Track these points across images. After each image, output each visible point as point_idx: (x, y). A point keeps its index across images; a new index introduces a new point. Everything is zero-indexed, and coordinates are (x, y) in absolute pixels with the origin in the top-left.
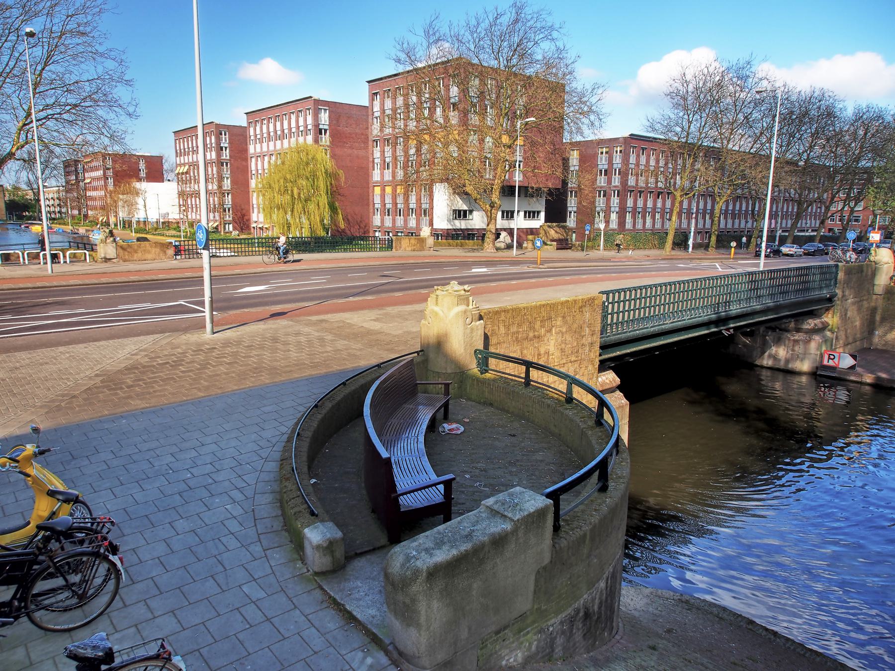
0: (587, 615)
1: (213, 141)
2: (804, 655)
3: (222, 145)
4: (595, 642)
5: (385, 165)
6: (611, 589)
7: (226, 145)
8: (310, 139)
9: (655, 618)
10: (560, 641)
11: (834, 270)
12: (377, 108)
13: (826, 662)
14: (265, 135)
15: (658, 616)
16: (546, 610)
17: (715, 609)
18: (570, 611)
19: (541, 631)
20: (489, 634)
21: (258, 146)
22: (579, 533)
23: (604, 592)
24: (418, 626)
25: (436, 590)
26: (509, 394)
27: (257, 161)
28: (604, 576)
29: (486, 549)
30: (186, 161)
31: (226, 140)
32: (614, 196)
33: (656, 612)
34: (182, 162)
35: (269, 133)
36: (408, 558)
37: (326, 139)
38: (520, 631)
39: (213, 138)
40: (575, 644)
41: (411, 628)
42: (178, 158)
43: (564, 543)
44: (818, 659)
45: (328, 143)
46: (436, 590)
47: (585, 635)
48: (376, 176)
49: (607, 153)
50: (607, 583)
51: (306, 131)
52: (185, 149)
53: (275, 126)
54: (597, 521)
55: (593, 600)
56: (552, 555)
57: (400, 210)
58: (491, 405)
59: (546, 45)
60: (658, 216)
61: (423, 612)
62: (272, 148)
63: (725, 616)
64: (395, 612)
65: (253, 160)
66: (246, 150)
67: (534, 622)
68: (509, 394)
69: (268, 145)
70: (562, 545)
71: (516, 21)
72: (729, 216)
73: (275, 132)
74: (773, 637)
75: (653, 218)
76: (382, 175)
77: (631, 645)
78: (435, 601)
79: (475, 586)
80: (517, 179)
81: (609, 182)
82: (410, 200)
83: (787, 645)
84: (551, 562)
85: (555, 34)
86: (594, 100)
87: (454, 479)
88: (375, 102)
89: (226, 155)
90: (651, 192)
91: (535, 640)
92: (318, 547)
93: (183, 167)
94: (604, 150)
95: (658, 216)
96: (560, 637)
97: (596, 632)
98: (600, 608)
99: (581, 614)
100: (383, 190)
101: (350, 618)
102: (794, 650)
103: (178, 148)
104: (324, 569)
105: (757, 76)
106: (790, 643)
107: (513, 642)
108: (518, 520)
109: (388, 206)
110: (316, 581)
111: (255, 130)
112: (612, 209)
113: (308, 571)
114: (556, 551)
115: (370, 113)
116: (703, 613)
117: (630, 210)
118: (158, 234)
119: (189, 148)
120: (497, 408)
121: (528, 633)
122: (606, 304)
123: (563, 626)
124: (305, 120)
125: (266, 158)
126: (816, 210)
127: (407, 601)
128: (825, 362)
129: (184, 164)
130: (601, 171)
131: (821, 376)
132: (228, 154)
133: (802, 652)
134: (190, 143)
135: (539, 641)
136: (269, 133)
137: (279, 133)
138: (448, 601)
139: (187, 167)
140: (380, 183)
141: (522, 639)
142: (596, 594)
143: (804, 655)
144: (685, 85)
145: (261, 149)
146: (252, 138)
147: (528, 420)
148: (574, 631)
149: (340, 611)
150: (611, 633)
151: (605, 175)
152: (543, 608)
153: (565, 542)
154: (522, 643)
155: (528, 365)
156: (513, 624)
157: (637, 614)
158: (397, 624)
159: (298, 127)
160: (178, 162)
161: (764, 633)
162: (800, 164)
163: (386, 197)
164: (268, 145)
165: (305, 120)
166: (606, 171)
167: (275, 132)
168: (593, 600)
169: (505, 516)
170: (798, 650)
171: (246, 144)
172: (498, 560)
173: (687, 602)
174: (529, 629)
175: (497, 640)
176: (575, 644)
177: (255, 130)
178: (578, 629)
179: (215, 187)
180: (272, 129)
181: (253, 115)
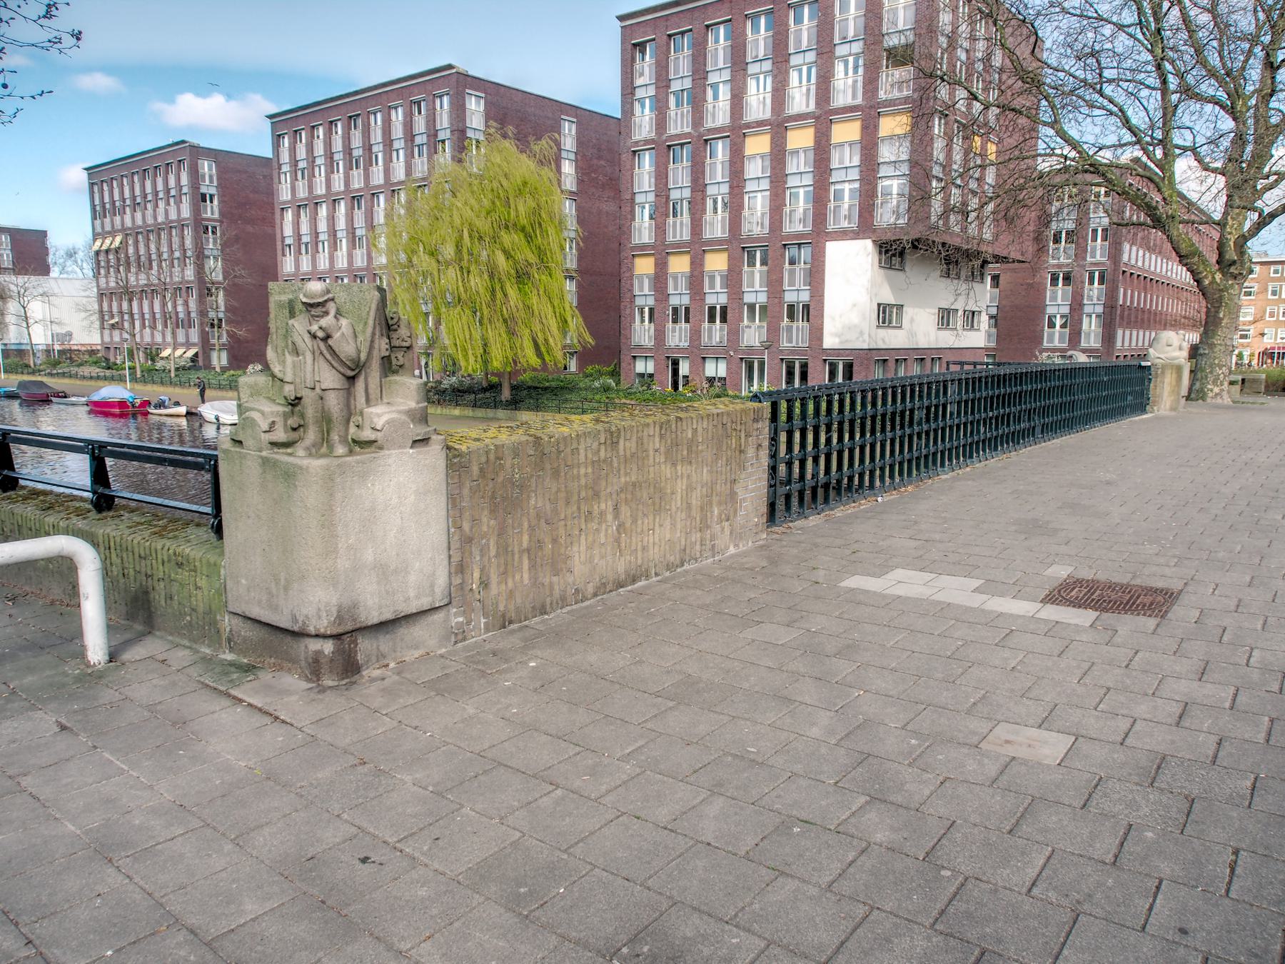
3: (203, 190)
7: (213, 191)
12: (285, 157)
27: (297, 216)
31: (211, 181)
32: (643, 321)
42: (98, 222)
65: (289, 216)
89: (212, 211)
93: (108, 242)
103: (97, 202)
115: (275, 165)
118: (63, 375)
119: (124, 200)
125: (323, 211)
129: (113, 233)
132: (216, 210)
139: (118, 239)
146: (285, 168)
151: (724, 320)
160: (99, 229)
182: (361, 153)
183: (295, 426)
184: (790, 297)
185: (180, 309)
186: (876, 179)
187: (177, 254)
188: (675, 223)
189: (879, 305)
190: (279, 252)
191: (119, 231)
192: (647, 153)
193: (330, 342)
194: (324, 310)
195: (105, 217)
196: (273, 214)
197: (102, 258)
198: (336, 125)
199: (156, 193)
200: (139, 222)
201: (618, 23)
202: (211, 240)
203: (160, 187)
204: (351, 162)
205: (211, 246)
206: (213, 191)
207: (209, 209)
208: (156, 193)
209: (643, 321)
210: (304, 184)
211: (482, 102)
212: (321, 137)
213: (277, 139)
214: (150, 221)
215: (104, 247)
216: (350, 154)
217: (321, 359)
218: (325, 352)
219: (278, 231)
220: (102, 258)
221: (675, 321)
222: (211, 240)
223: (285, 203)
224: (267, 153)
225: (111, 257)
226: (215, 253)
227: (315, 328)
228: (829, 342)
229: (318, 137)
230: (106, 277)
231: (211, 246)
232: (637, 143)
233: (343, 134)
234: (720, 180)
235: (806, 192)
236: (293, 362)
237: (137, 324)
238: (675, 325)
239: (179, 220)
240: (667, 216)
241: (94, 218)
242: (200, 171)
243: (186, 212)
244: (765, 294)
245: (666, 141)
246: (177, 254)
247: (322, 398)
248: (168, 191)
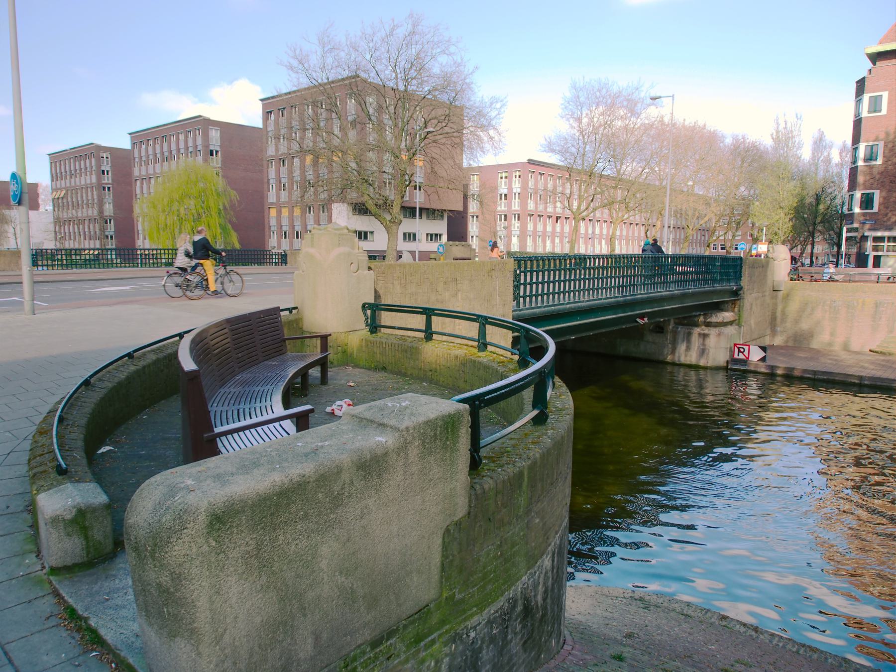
0: (528, 611)
1: (93, 164)
2: (797, 652)
4: (539, 656)
5: (281, 186)
6: (557, 572)
7: (109, 169)
8: (200, 158)
9: (606, 622)
10: (487, 654)
11: (739, 261)
13: (826, 659)
14: (151, 157)
15: (609, 619)
16: (462, 601)
17: (676, 605)
18: (501, 603)
19: (456, 638)
20: (359, 646)
21: (143, 168)
22: (511, 470)
23: (550, 574)
24: (193, 633)
25: (234, 554)
26: (406, 351)
27: (142, 184)
28: (550, 548)
29: (345, 477)
30: (63, 186)
31: (107, 164)
32: (515, 220)
33: (606, 614)
34: (59, 186)
35: (155, 155)
36: (172, 491)
37: (217, 161)
38: (418, 639)
39: (93, 160)
40: (510, 659)
41: (178, 639)
42: (54, 183)
43: (488, 483)
44: (815, 656)
45: (220, 165)
46: (234, 554)
47: (525, 642)
48: (271, 197)
49: (506, 177)
50: (553, 561)
51: (196, 151)
52: (61, 173)
53: (162, 148)
54: (538, 455)
55: (535, 586)
56: (470, 501)
57: (297, 232)
58: (384, 369)
59: (443, 59)
60: (557, 240)
61: (202, 603)
62: (158, 170)
63: (690, 612)
64: (147, 611)
65: (138, 183)
66: (129, 174)
67: (443, 622)
68: (406, 351)
69: (154, 167)
70: (486, 487)
71: (413, 33)
72: (623, 242)
73: (163, 153)
74: (754, 633)
75: (553, 242)
76: (278, 196)
77: (588, 657)
78: (234, 579)
79: (324, 550)
80: (418, 200)
81: (510, 206)
82: (307, 221)
83: (775, 642)
84: (469, 513)
85: (452, 49)
86: (493, 114)
87: (312, 411)
88: (269, 121)
89: (107, 180)
90: (550, 217)
91: (446, 655)
92: (55, 521)
93: (59, 193)
94: (504, 175)
95: (557, 240)
96: (488, 647)
97: (540, 639)
98: (544, 599)
99: (519, 608)
100: (279, 213)
101: (95, 640)
102: (784, 647)
104: (69, 562)
105: (645, 101)
106: (777, 639)
107: (407, 661)
108: (407, 428)
109: (284, 229)
110: (50, 582)
111: (140, 151)
112: (514, 233)
113: (44, 568)
114: (476, 495)
116: (664, 611)
117: (531, 233)
120: (392, 372)
121: (433, 642)
122: (518, 272)
123: (492, 628)
124: (195, 140)
125: (297, 161)
126: (701, 238)
127: (165, 579)
128: (736, 356)
129: (61, 189)
130: (501, 195)
131: (732, 370)
133: (794, 650)
134: (90, 194)
135: (452, 655)
136: (155, 155)
137: (166, 154)
138: (264, 578)
139: (64, 192)
140: (275, 204)
141: (423, 654)
142: (539, 577)
143: (797, 652)
144: (579, 108)
145: (147, 172)
146: (137, 160)
147: (431, 381)
148: (509, 637)
149: (79, 630)
150: (558, 642)
151: (506, 199)
152: (458, 596)
153: (491, 481)
154: (423, 661)
155: (428, 313)
156: (405, 627)
157: (581, 618)
158: (152, 635)
159: (187, 148)
160: (54, 187)
161: (743, 629)
162: (689, 184)
163: (282, 220)
164: (154, 167)
165: (195, 140)
166: (506, 195)
167: (163, 153)
168: (535, 586)
169: (384, 425)
170: (789, 646)
171: (130, 168)
172: (371, 502)
173: (641, 599)
174: (435, 635)
175: (376, 658)
176: (510, 659)
177: (140, 151)
178: (516, 634)
179: (96, 213)
180: (158, 150)
181: (139, 138)
191: (63, 188)
195: (57, 180)
197: (56, 201)
199: (81, 169)
200: (73, 184)
201: (261, 102)
203: (83, 166)
207: (106, 178)
208: (81, 169)
209: (515, 220)
211: (219, 132)
214: (78, 184)
215: (57, 197)
216: (164, 155)
220: (56, 201)
224: (258, 123)
225: (60, 201)
230: (63, 213)
231: (107, 197)
233: (275, 120)
239: (91, 184)
241: (52, 180)
243: (94, 180)
248: (86, 168)
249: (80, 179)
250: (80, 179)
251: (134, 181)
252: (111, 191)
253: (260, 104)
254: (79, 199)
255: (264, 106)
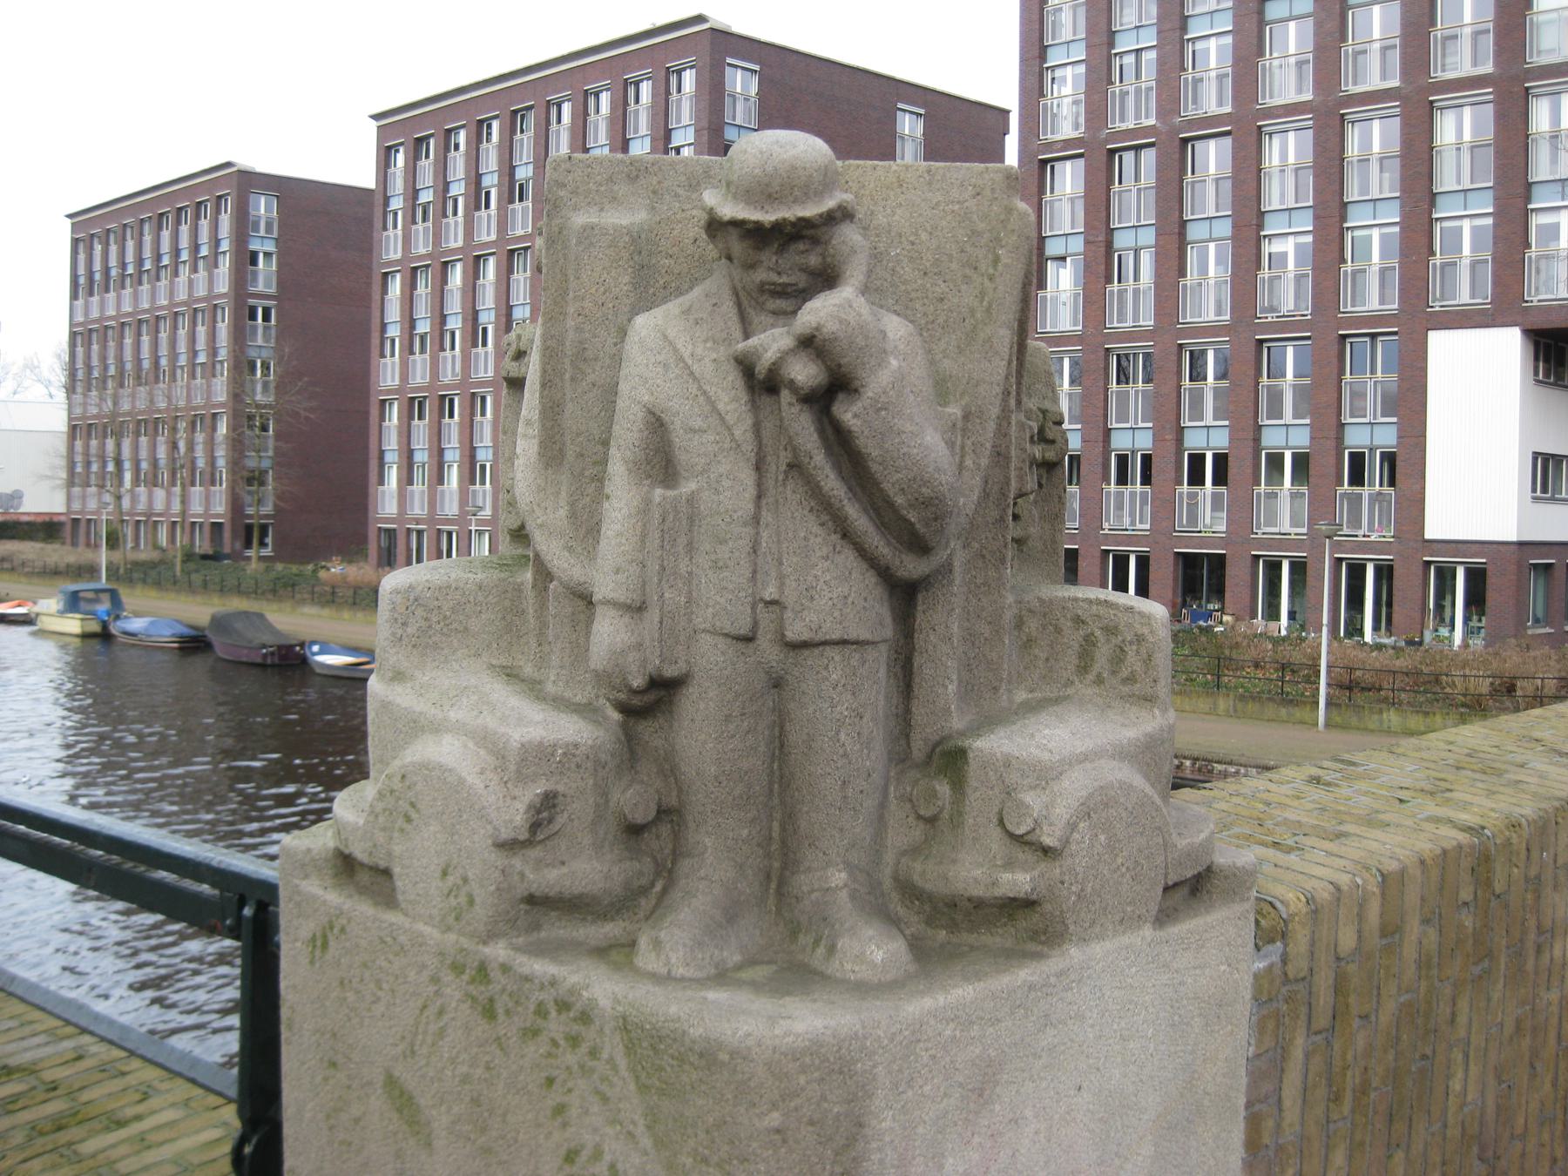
12: (398, 184)
65: (396, 287)
89: (265, 276)
115: (379, 199)
145: (211, 288)
151: (1220, 478)
182: (530, 174)
183: (639, 817)
184: (1356, 438)
185: (200, 452)
186: (1526, 214)
187: (202, 358)
188: (1122, 293)
189: (1536, 455)
190: (375, 351)
192: (1068, 164)
193: (848, 413)
194: (814, 260)
196: (369, 285)
198: (489, 126)
199: (176, 252)
201: (374, 124)
202: (260, 331)
204: (511, 192)
205: (260, 342)
206: (270, 247)
210: (426, 230)
212: (462, 147)
213: (385, 155)
217: (792, 495)
218: (819, 461)
219: (376, 313)
221: (1122, 479)
222: (260, 331)
223: (390, 264)
224: (365, 177)
226: (265, 354)
227: (772, 342)
228: (1438, 526)
229: (457, 147)
231: (260, 342)
232: (1050, 146)
234: (1213, 213)
235: (1383, 237)
236: (645, 508)
237: (128, 476)
238: (1122, 488)
240: (1109, 280)
241: (74, 296)
242: (252, 212)
244: (1307, 431)
245: (1107, 141)
246: (202, 358)
247: (777, 684)
249: (172, 283)
250: (172, 283)
251: (377, 280)
252: (273, 322)
253: (69, 222)
254: (164, 350)
255: (75, 227)
